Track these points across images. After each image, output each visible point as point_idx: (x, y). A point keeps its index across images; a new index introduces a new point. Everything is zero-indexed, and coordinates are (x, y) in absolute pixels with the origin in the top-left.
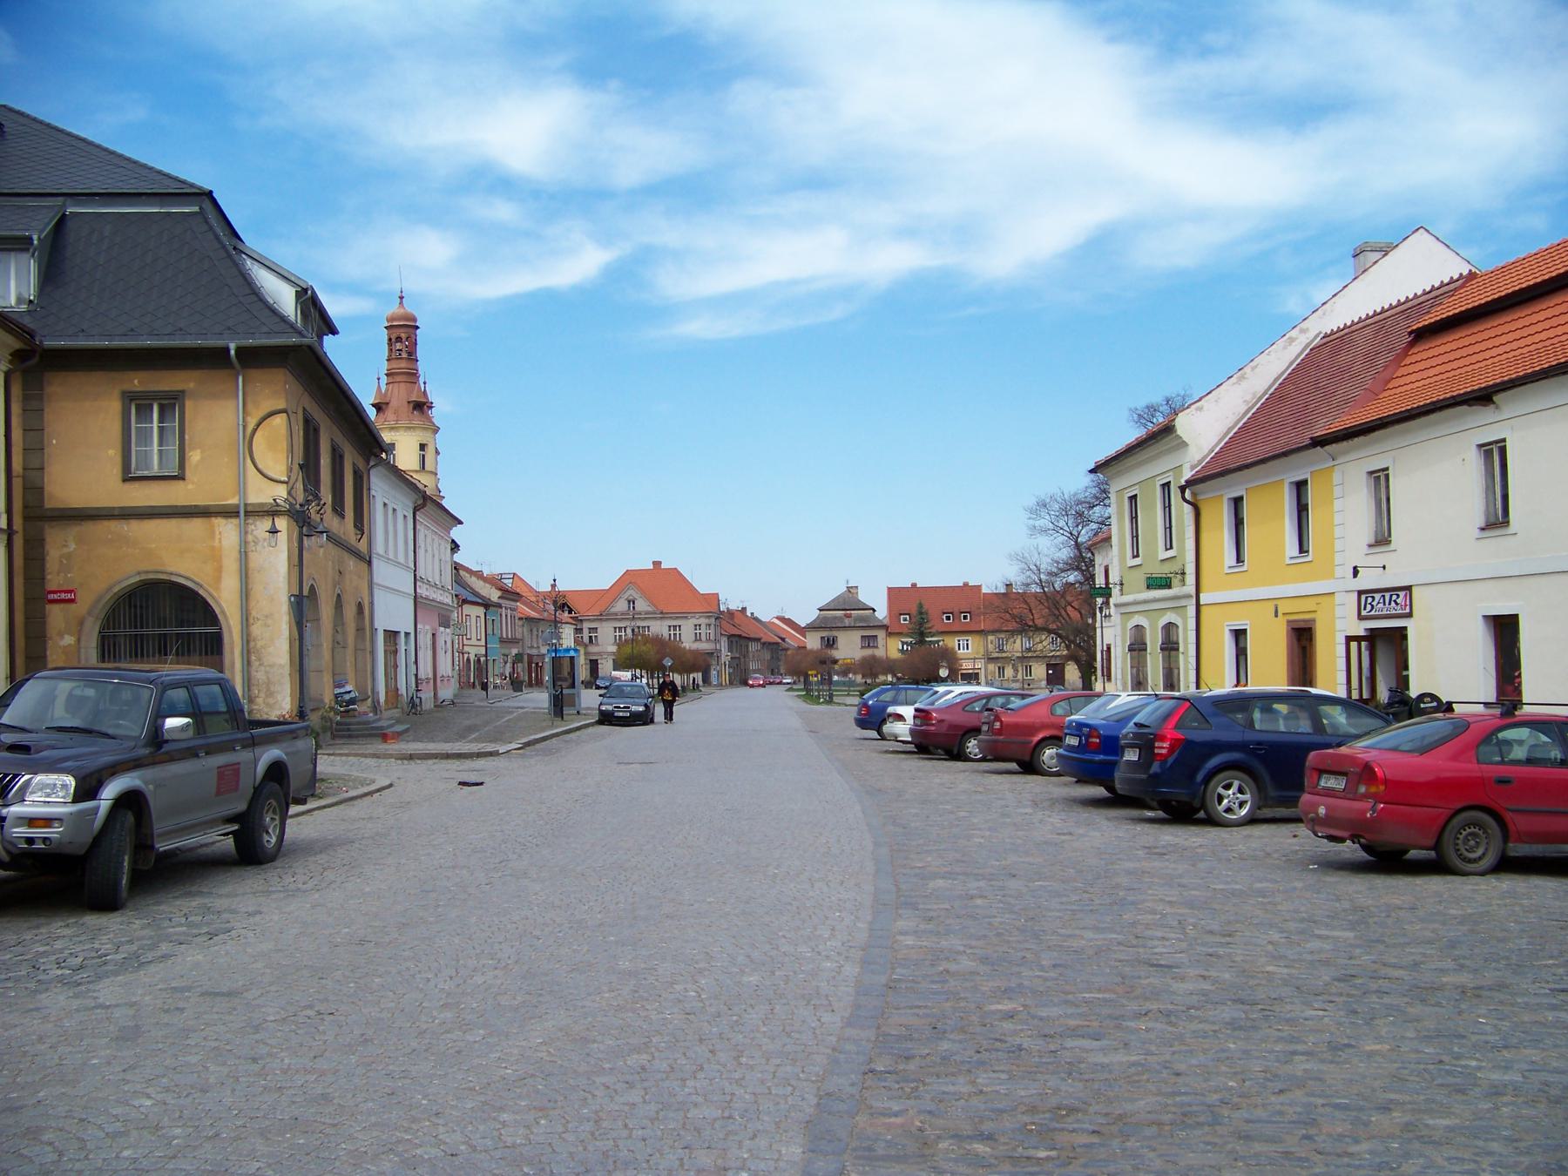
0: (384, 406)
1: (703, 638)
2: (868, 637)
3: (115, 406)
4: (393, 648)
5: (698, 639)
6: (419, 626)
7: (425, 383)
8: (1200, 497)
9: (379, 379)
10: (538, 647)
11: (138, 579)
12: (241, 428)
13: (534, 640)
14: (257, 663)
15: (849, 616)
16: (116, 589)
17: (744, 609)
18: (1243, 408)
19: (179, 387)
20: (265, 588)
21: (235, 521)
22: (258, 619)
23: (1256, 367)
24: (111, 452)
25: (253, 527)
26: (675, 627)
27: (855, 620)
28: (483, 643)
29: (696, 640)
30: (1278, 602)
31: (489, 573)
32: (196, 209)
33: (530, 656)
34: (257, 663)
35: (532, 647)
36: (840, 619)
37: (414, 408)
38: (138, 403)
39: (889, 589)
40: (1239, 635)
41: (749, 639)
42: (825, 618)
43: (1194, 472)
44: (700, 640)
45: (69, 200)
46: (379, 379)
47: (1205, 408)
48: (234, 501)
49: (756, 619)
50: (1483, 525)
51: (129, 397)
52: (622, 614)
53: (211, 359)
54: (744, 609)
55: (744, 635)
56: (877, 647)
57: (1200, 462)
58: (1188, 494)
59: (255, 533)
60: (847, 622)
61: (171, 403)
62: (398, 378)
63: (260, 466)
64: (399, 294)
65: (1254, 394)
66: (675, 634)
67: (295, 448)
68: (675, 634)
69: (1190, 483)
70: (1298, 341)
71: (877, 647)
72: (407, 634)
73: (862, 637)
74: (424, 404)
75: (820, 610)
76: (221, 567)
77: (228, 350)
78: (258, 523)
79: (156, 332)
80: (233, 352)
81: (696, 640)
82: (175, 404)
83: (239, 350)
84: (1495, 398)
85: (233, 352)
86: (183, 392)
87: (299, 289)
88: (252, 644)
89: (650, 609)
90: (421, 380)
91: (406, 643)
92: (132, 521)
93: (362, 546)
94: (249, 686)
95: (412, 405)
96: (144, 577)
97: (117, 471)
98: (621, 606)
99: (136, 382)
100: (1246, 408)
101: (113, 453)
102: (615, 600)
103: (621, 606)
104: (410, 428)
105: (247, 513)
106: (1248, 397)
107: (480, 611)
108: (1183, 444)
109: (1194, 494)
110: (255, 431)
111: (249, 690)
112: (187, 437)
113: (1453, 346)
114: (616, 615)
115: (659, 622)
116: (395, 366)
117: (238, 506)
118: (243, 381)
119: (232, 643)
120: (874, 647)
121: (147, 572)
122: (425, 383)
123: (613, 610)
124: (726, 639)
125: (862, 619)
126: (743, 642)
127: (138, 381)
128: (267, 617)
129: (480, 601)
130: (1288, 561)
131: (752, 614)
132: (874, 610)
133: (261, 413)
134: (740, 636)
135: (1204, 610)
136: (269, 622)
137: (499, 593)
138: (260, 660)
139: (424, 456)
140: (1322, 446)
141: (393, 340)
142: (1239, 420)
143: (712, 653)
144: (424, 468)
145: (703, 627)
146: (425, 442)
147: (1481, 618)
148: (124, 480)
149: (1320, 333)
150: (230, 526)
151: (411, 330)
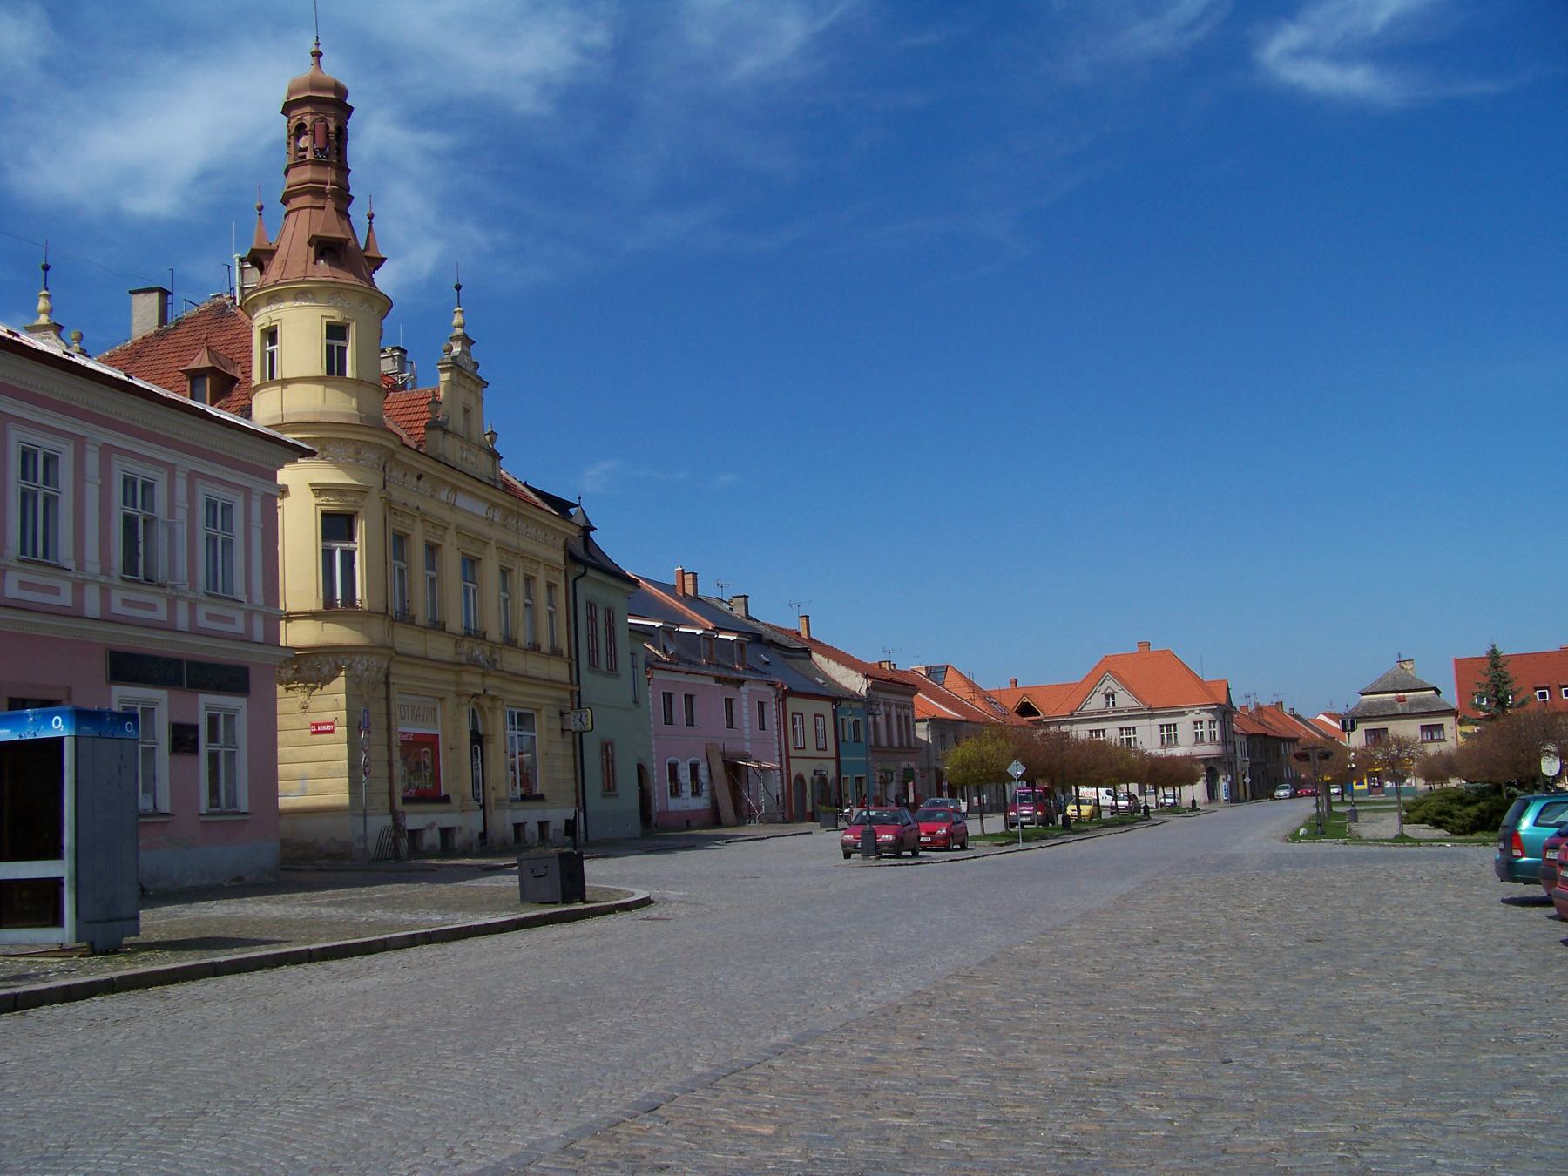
2: (1374, 731)
5: (1198, 739)
15: (1402, 700)
26: (1168, 726)
27: (1412, 704)
28: (831, 752)
29: (1197, 742)
36: (1390, 704)
39: (1456, 660)
44: (1202, 741)
52: (1099, 713)
55: (1271, 733)
56: (1444, 740)
60: (1400, 708)
66: (1169, 737)
67: (436, 920)
68: (1169, 737)
71: (1444, 740)
89: (1134, 704)
91: (551, 603)
98: (1096, 703)
102: (1089, 694)
114: (1091, 714)
115: (1147, 721)
119: (70, 904)
120: (1439, 740)
123: (1087, 708)
124: (1244, 739)
125: (1420, 702)
132: (1438, 692)
134: (1265, 735)
145: (1206, 724)
146: (520, 821)
148: (748, 597)
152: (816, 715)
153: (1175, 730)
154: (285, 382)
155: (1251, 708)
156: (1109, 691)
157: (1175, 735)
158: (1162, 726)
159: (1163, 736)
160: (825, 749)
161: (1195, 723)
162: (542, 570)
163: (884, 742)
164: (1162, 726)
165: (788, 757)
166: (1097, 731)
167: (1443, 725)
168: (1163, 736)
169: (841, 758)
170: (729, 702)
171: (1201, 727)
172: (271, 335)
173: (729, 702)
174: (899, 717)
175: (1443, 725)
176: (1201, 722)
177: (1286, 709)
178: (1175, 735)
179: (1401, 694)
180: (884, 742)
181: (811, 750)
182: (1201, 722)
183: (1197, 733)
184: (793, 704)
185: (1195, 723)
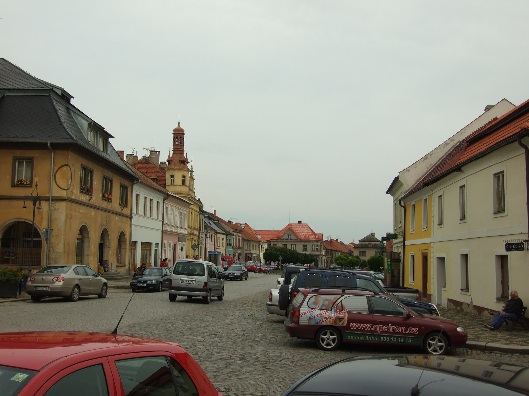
0: (171, 162)
1: (315, 250)
3: (10, 160)
4: (150, 249)
6: (165, 241)
7: (187, 154)
8: (406, 204)
9: (169, 152)
10: (250, 251)
11: (14, 220)
12: (52, 170)
13: (248, 247)
14: (52, 252)
15: (371, 244)
16: (7, 224)
17: (337, 240)
18: (426, 170)
19: (32, 156)
20: (57, 226)
21: (48, 202)
22: (54, 236)
23: (432, 154)
24: (8, 177)
25: (54, 204)
26: (305, 245)
28: (225, 248)
29: (313, 250)
30: (421, 245)
31: (236, 222)
32: (48, 94)
33: (246, 254)
34: (52, 252)
35: (247, 250)
36: (367, 245)
37: (181, 163)
38: (19, 160)
40: (413, 256)
41: (337, 251)
42: (362, 245)
43: (405, 195)
44: (314, 250)
45: (6, 91)
46: (169, 152)
47: (410, 170)
48: (48, 195)
49: (343, 244)
50: (461, 218)
51: (15, 159)
53: (41, 146)
54: (337, 240)
57: (408, 191)
58: (402, 203)
59: (55, 206)
60: (370, 246)
61: (30, 162)
62: (177, 152)
63: (58, 184)
64: (178, 122)
65: (431, 165)
66: (305, 248)
68: (305, 248)
69: (403, 198)
70: (450, 144)
72: (157, 244)
73: (360, 252)
74: (185, 161)
75: (360, 241)
76: (43, 218)
77: (47, 143)
78: (56, 203)
79: (25, 137)
80: (49, 144)
81: (313, 250)
82: (24, 161)
83: (51, 144)
84: (462, 169)
85: (49, 144)
86: (33, 157)
87: (89, 123)
88: (51, 245)
90: (185, 153)
92: (13, 201)
93: (126, 211)
94: (49, 259)
95: (180, 162)
96: (16, 220)
97: (9, 184)
98: (286, 237)
99: (18, 153)
100: (427, 170)
101: (9, 177)
103: (286, 237)
104: (179, 170)
105: (52, 200)
106: (428, 166)
107: (224, 236)
108: (402, 184)
109: (405, 203)
110: (57, 172)
111: (48, 261)
112: (34, 173)
113: (476, 147)
116: (176, 148)
117: (49, 197)
118: (54, 155)
121: (18, 218)
122: (187, 154)
126: (333, 252)
127: (18, 153)
128: (57, 236)
129: (224, 233)
130: (423, 230)
131: (341, 241)
133: (59, 166)
134: (332, 250)
135: (406, 248)
136: (58, 237)
137: (233, 230)
138: (53, 250)
139: (184, 180)
140: (428, 186)
141: (175, 138)
142: (424, 175)
143: (319, 256)
144: (184, 184)
145: (315, 245)
146: (185, 175)
147: (495, 256)
149: (459, 141)
150: (47, 204)
151: (181, 135)
152: (222, 238)
153: (307, 246)
154: (175, 185)
155: (329, 240)
156: (289, 234)
157: (307, 248)
158: (303, 245)
159: (303, 248)
160: (223, 247)
161: (313, 245)
162: (193, 211)
163: (235, 246)
164: (303, 245)
165: (216, 249)
166: (285, 245)
167: (365, 252)
168: (303, 248)
169: (227, 249)
170: (466, 289)
171: (314, 247)
172: (172, 176)
173: (466, 289)
174: (238, 239)
175: (365, 252)
176: (314, 245)
177: (339, 241)
178: (307, 248)
179: (370, 242)
180: (235, 246)
181: (221, 247)
182: (314, 245)
183: (313, 248)
184: (218, 235)
185: (313, 245)
